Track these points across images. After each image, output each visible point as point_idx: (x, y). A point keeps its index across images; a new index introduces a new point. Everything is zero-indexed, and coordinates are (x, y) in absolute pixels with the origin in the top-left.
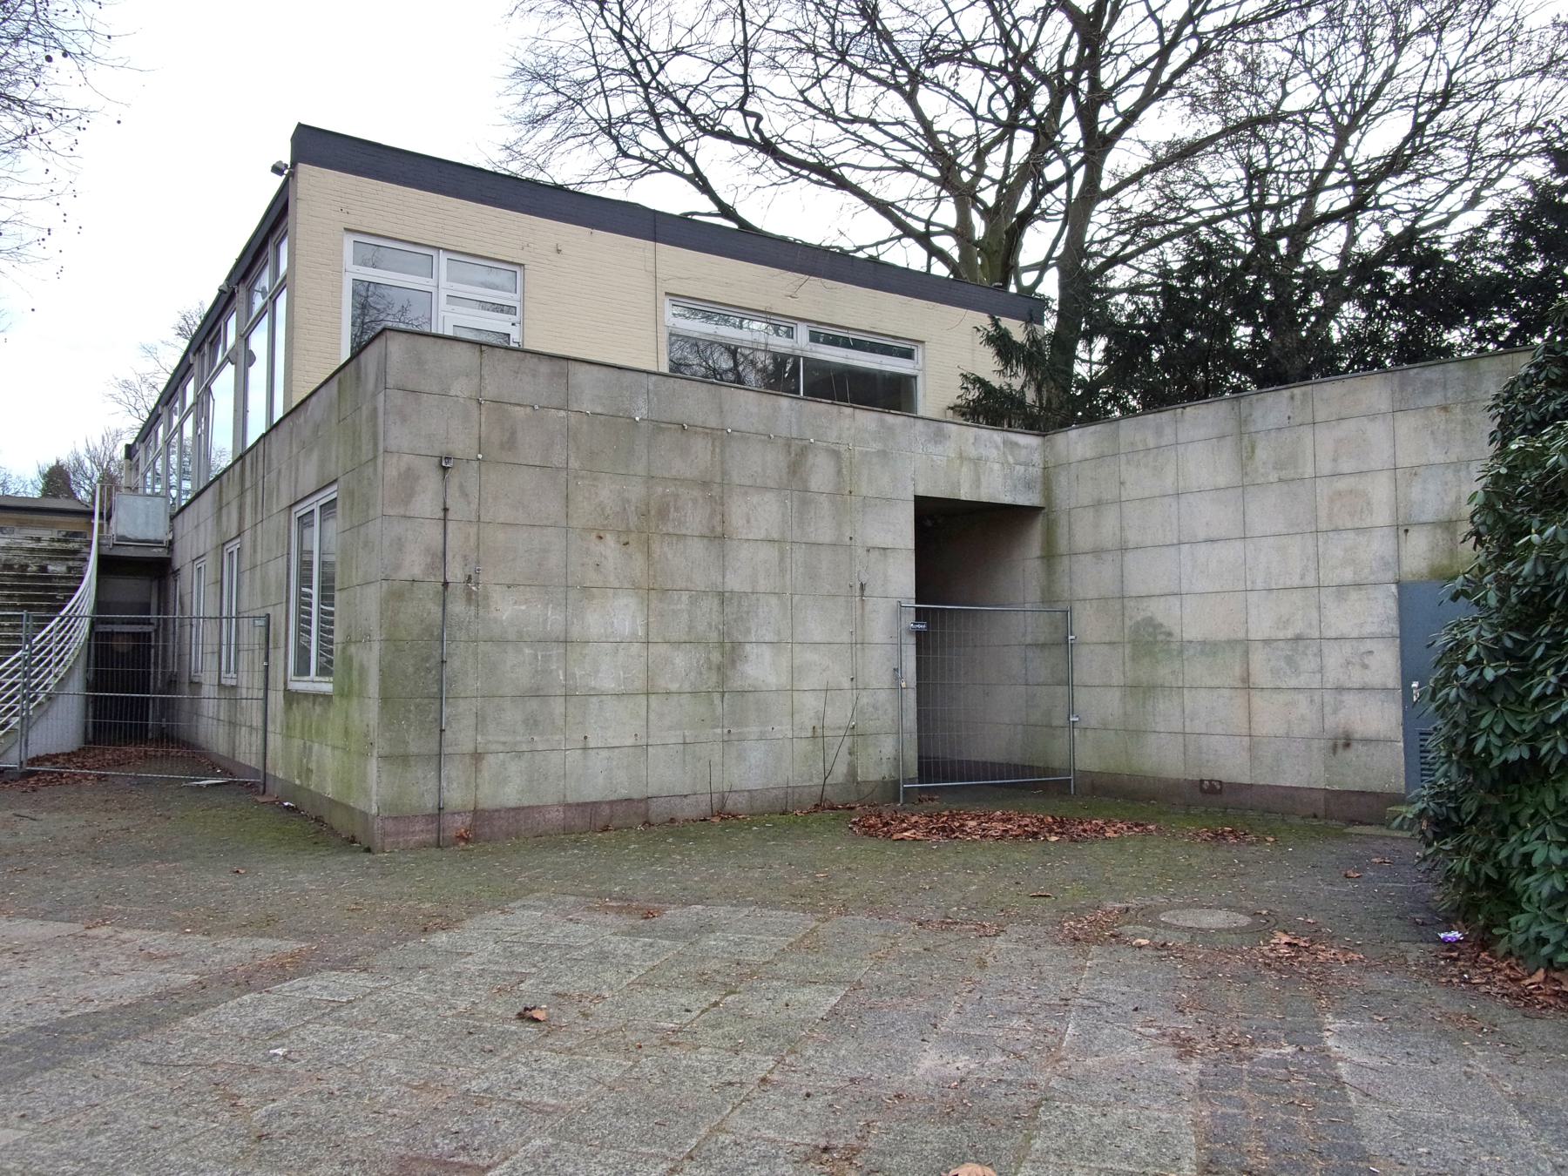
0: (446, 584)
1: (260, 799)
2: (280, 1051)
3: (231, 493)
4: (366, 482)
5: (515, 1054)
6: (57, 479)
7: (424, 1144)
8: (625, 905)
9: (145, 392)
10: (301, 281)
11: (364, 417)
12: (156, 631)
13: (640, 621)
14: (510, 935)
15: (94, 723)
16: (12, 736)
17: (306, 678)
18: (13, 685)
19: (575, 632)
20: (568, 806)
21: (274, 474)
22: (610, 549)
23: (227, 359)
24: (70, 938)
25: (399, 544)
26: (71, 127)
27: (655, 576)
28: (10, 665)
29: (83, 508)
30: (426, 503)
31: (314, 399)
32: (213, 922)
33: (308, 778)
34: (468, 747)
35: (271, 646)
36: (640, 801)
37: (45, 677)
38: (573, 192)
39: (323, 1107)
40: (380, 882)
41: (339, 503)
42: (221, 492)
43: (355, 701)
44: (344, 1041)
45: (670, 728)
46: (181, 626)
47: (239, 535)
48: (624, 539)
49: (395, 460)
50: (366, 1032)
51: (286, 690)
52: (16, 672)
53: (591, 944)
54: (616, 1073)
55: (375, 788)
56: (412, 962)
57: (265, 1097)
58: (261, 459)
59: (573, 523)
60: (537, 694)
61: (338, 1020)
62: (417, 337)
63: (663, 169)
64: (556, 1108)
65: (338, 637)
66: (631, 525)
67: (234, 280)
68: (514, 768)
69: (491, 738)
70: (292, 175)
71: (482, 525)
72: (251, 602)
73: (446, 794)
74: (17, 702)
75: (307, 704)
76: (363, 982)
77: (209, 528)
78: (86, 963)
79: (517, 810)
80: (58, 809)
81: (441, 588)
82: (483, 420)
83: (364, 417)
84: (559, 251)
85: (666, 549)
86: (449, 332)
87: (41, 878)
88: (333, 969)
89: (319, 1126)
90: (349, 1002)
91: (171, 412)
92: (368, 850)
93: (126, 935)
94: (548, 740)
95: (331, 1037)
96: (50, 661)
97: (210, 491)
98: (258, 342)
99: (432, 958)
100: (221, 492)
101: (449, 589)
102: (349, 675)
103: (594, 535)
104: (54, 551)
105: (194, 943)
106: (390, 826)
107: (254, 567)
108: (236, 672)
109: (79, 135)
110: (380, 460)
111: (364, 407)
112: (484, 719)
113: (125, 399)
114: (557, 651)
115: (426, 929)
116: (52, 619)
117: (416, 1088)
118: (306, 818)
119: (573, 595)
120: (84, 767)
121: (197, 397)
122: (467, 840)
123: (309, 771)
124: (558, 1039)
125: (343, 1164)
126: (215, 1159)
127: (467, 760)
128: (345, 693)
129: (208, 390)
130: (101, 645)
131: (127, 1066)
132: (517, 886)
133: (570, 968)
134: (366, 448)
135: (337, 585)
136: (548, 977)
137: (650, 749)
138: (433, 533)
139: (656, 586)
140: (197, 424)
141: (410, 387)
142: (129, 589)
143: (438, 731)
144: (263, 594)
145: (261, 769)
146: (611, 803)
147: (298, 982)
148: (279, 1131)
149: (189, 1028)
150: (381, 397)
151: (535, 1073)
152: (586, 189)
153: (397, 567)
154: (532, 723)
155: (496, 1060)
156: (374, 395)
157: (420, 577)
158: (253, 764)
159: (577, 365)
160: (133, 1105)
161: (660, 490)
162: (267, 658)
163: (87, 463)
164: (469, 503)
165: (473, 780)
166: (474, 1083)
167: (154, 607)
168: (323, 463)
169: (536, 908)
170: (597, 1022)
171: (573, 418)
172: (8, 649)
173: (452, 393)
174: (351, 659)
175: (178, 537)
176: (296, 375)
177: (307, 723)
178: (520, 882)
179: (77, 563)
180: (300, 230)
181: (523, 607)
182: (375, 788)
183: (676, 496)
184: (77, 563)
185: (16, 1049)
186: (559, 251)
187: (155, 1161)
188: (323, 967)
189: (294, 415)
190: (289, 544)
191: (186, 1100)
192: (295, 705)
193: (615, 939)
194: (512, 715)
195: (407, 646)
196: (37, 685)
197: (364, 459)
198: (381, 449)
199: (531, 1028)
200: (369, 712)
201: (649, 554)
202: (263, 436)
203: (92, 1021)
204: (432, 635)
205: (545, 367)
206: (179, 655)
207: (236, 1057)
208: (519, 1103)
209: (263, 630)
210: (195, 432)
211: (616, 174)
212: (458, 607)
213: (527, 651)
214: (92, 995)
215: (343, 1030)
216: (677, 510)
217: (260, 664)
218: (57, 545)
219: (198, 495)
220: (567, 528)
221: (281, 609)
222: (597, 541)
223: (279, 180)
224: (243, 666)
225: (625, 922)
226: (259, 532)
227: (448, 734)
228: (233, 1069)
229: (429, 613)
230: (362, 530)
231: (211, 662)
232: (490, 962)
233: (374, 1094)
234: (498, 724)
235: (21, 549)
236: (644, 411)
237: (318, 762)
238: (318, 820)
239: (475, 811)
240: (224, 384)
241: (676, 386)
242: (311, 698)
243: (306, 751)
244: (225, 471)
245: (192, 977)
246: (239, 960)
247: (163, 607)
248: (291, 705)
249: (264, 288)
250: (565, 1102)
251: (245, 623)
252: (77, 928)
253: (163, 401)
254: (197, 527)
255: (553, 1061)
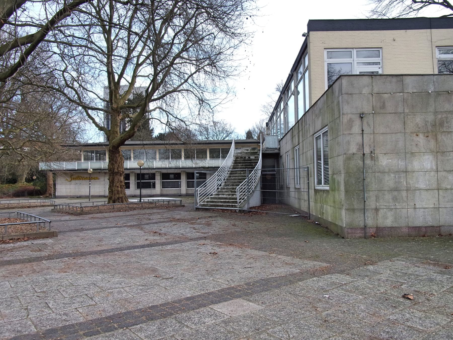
0: (364, 154)
1: (309, 221)
2: (327, 296)
3: (296, 133)
4: (337, 124)
5: (404, 309)
6: (249, 134)
7: (377, 333)
8: (436, 263)
9: (269, 108)
10: (312, 67)
11: (335, 104)
12: (277, 173)
13: (434, 163)
14: (395, 269)
15: (263, 198)
16: (245, 202)
17: (321, 185)
18: (245, 188)
19: (409, 168)
20: (409, 228)
21: (308, 125)
22: (421, 139)
23: (292, 94)
24: (266, 256)
25: (348, 143)
26: (250, 38)
27: (439, 147)
28: (244, 183)
29: (256, 141)
30: (356, 129)
31: (319, 101)
32: (301, 255)
33: (323, 215)
34: (373, 207)
35: (309, 176)
36: (437, 227)
37: (252, 186)
38: (397, 19)
39: (342, 315)
40: (348, 248)
41: (329, 132)
42: (293, 133)
43: (337, 192)
44: (346, 296)
45: (448, 202)
46: (283, 172)
47: (298, 145)
48: (426, 135)
49: (346, 117)
50: (352, 294)
51: (315, 189)
52: (245, 185)
53: (426, 275)
54: (444, 323)
55: (344, 219)
56: (363, 274)
57: (325, 309)
58: (304, 121)
59: (407, 131)
60: (396, 189)
61: (343, 289)
62: (362, 76)
63: (430, 3)
64: (423, 331)
65: (330, 173)
66: (429, 129)
67: (293, 71)
68: (390, 214)
69: (381, 204)
70: (308, 36)
71: (375, 134)
72: (303, 163)
73: (367, 221)
74: (246, 193)
75: (321, 193)
76: (348, 278)
77: (290, 144)
78: (271, 264)
79: (391, 228)
80: (258, 221)
81: (362, 155)
82: (374, 100)
83: (335, 104)
84: (394, 40)
85: (443, 137)
86: (358, 73)
87: (256, 239)
88: (338, 273)
89: (342, 321)
90: (345, 284)
91: (277, 112)
92: (343, 238)
93: (279, 257)
94: (401, 205)
95: (341, 294)
96: (253, 182)
97: (289, 133)
98: (300, 87)
99: (369, 274)
100: (293, 133)
101: (365, 156)
102: (334, 184)
103: (415, 135)
104: (251, 153)
105: (297, 261)
106: (350, 231)
107: (303, 154)
108: (300, 184)
109: (252, 39)
110: (341, 117)
111: (335, 101)
112: (378, 198)
113: (264, 110)
114: (403, 175)
115: (365, 264)
116: (252, 171)
117: (371, 314)
118: (323, 227)
119: (408, 156)
120: (262, 210)
121: (284, 106)
122: (375, 237)
123: (323, 213)
124: (419, 307)
125: (352, 334)
126: (314, 325)
127: (374, 211)
128: (333, 189)
129: (287, 104)
130: (264, 177)
131: (286, 294)
132: (394, 253)
133: (419, 283)
134: (336, 116)
135: (329, 157)
136: (412, 284)
137: (440, 209)
138: (359, 138)
139: (440, 151)
140: (284, 114)
141: (350, 93)
142: (270, 162)
143: (363, 201)
144: (306, 161)
145: (308, 212)
146: (426, 227)
147: (329, 276)
148: (331, 320)
149: (300, 285)
150: (341, 97)
151: (413, 317)
152: (401, 17)
153: (348, 150)
154: (395, 199)
155: (397, 310)
156: (339, 97)
157: (355, 152)
158: (306, 211)
159: (406, 77)
160: (289, 305)
161: (440, 116)
162: (308, 180)
163: (256, 129)
164: (370, 128)
165: (376, 218)
166: (391, 316)
167: (276, 166)
168: (323, 120)
169: (402, 261)
170: (433, 303)
171: (406, 95)
172: (243, 179)
173: (363, 93)
174: (334, 179)
175: (281, 147)
176: (312, 95)
177: (322, 199)
178: (395, 252)
179: (257, 156)
180: (311, 51)
181: (390, 161)
182: (344, 219)
183: (447, 118)
184: (257, 156)
185: (258, 284)
186: (394, 40)
187: (297, 322)
188: (335, 272)
189: (313, 107)
190: (313, 146)
191: (303, 306)
192: (318, 194)
193: (435, 274)
194: (388, 197)
195: (352, 175)
196: (250, 188)
197: (336, 117)
198: (341, 113)
199: (408, 301)
200: (341, 195)
201: (436, 139)
202: (304, 115)
203: (275, 280)
204: (360, 171)
205: (394, 79)
206: (283, 180)
207: (314, 296)
208: (408, 326)
209: (307, 172)
210: (284, 116)
211: (412, 10)
212: (368, 162)
213: (392, 175)
214: (274, 273)
215: (345, 292)
216: (447, 122)
217: (306, 182)
218: (252, 151)
219: (286, 134)
220: (405, 133)
221: (312, 165)
222: (416, 137)
223: (304, 38)
224: (301, 182)
225: (438, 269)
226: (304, 143)
227: (367, 202)
228: (314, 299)
229: (359, 164)
230: (337, 139)
231: (292, 182)
232: (389, 277)
233: (358, 314)
234: (383, 199)
235: (244, 153)
236: (432, 89)
237: (326, 210)
238: (327, 228)
239: (377, 227)
240: (291, 102)
241: (445, 78)
242: (323, 191)
243: (322, 207)
244: (293, 127)
245: (298, 271)
246: (310, 267)
247: (278, 166)
248: (316, 193)
249: (301, 72)
250: (285, 302)
251: (301, 170)
252: (267, 253)
253: (275, 109)
254: (286, 143)
255: (418, 314)
